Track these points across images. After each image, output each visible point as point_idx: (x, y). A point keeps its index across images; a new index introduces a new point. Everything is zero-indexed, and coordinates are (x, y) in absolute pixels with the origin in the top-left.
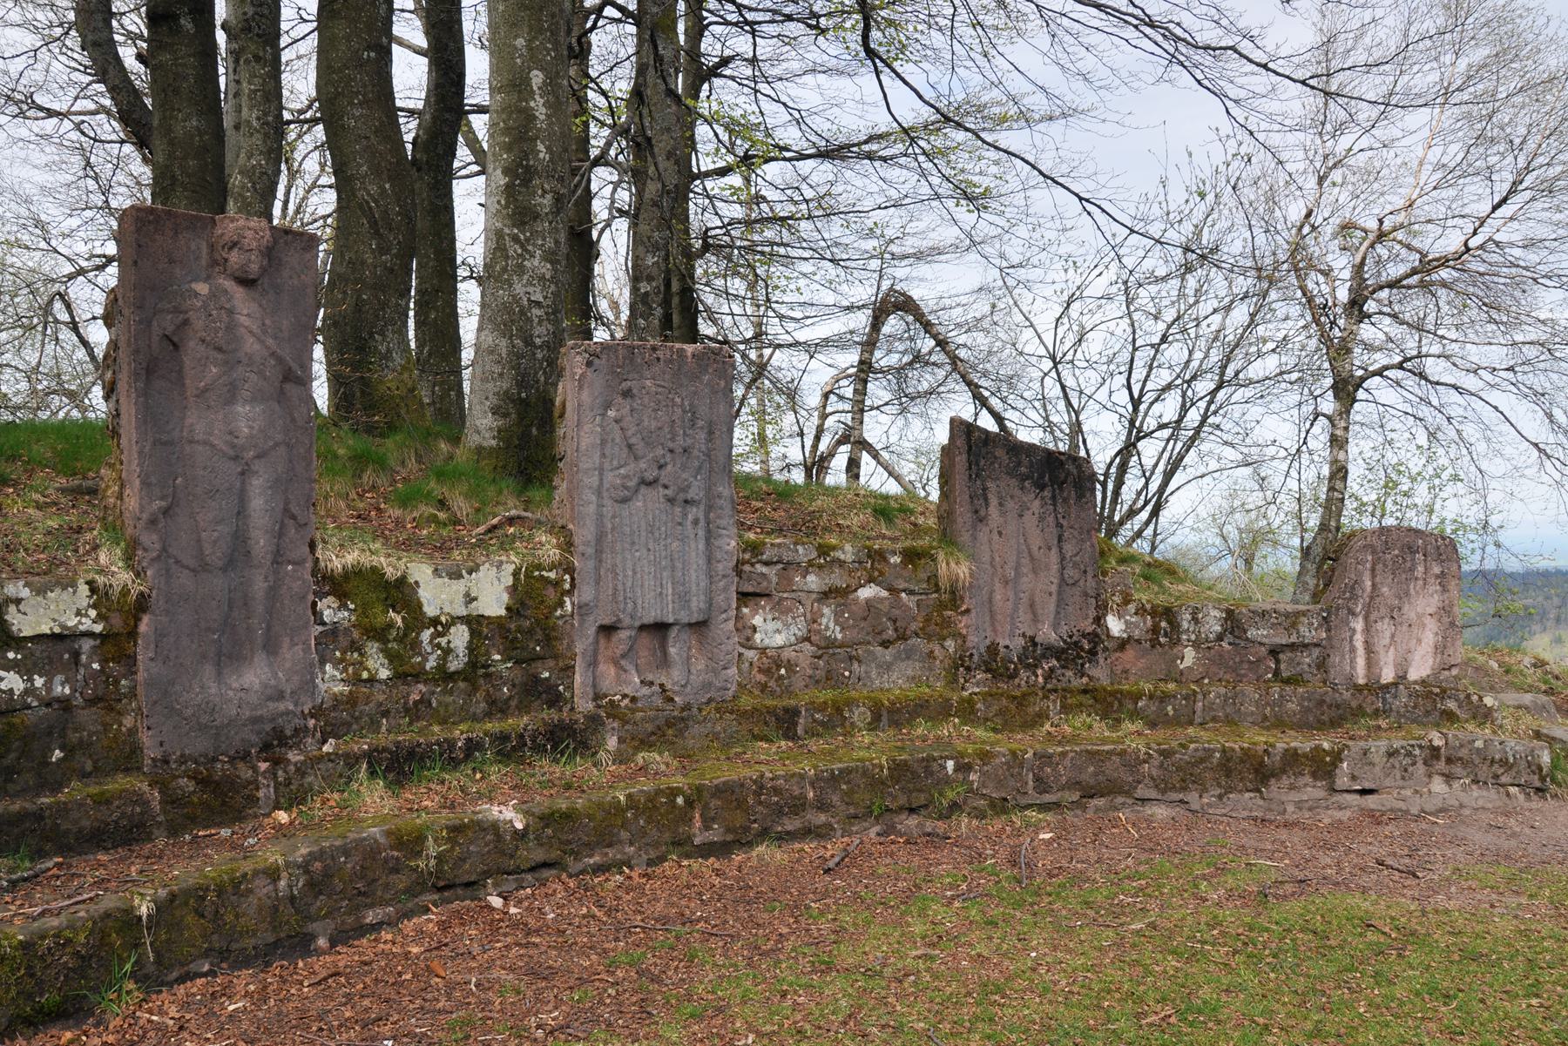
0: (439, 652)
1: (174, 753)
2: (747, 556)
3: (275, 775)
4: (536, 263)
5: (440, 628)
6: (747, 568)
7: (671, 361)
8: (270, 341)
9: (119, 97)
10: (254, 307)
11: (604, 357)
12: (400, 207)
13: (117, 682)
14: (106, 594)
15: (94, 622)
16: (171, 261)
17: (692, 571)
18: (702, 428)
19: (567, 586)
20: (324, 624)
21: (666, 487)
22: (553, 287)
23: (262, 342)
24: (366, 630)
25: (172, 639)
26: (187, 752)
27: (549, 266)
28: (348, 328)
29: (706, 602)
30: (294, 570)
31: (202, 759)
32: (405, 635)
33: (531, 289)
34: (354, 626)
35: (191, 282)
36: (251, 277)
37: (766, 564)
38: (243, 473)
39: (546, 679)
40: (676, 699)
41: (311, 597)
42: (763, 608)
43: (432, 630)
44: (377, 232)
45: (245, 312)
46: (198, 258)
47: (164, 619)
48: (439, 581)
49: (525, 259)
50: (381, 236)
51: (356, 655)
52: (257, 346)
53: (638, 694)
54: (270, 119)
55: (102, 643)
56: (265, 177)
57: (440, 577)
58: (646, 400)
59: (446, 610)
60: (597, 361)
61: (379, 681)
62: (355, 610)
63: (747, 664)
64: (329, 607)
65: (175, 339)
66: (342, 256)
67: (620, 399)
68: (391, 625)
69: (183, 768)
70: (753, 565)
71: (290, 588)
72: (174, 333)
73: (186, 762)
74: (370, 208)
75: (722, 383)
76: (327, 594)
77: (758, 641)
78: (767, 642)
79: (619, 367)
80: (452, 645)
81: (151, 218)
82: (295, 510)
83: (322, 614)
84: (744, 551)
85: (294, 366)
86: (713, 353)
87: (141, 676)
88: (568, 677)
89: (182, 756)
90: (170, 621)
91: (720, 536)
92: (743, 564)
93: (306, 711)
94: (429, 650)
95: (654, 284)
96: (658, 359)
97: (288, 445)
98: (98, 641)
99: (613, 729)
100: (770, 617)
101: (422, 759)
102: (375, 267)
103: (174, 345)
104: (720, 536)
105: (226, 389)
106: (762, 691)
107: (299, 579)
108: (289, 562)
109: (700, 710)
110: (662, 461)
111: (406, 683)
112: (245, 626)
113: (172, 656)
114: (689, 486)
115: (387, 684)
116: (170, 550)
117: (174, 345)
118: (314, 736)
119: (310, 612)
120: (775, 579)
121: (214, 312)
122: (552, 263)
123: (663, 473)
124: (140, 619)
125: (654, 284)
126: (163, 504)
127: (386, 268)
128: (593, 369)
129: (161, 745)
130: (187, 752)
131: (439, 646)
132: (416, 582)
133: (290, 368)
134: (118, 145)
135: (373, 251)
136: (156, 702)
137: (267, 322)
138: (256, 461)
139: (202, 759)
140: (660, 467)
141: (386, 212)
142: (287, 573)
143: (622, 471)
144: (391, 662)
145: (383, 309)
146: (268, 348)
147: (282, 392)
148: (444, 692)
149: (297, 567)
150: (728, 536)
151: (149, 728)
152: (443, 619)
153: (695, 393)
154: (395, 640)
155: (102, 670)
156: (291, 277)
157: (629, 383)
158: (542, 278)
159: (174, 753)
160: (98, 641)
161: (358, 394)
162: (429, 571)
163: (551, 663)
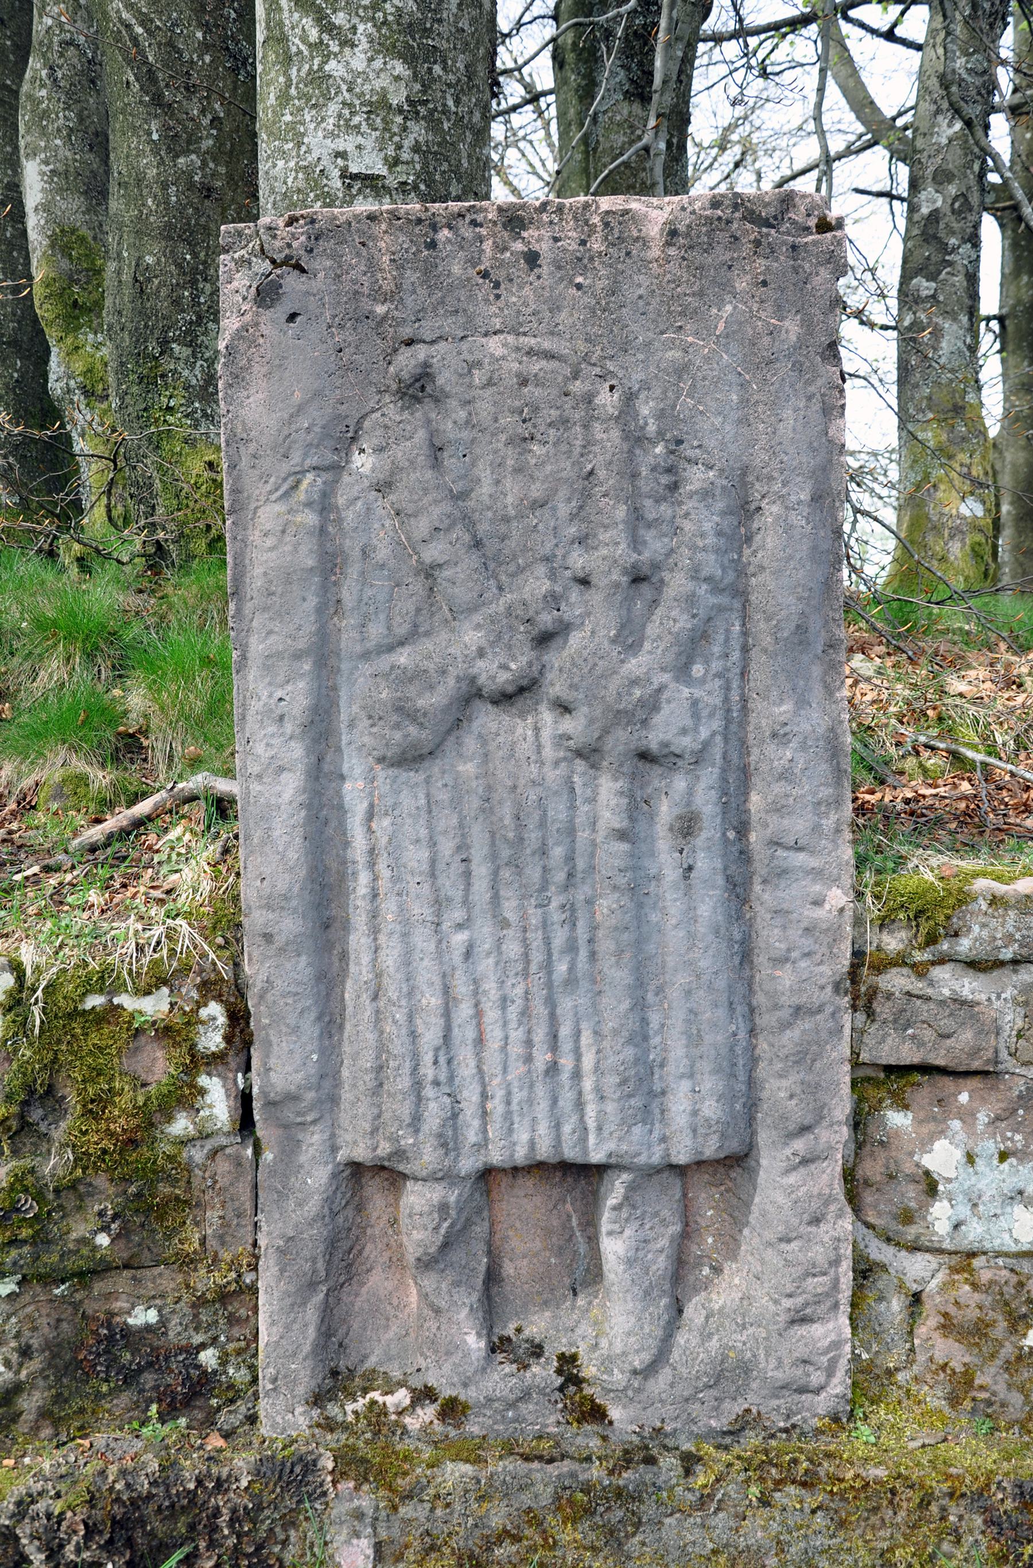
2: (893, 942)
4: (358, 61)
6: (897, 981)
7: (581, 262)
11: (320, 265)
12: (206, 28)
17: (674, 993)
18: (706, 494)
19: (212, 1040)
21: (564, 708)
22: (418, 132)
27: (399, 68)
29: (727, 1098)
33: (347, 143)
37: (974, 965)
39: (148, 1328)
40: (615, 1413)
42: (967, 1116)
49: (326, 59)
50: (168, 108)
53: (470, 1395)
56: (71, 51)
58: (484, 409)
60: (292, 281)
63: (896, 1304)
67: (392, 411)
70: (920, 971)
74: (135, 39)
75: (792, 328)
77: (942, 1228)
78: (974, 1232)
79: (379, 295)
84: (884, 923)
86: (752, 217)
88: (233, 1320)
91: (783, 872)
92: (881, 966)
95: (952, 190)
96: (532, 259)
99: (358, 1515)
100: (989, 1147)
102: (165, 186)
104: (783, 872)
106: (954, 1401)
109: (690, 1462)
110: (546, 619)
114: (652, 704)
120: (1012, 1019)
122: (409, 58)
123: (556, 658)
125: (952, 190)
127: (191, 185)
128: (281, 312)
140: (544, 639)
141: (171, 44)
143: (403, 658)
145: (194, 283)
150: (817, 874)
153: (681, 370)
157: (421, 352)
158: (379, 106)
163: (167, 1280)
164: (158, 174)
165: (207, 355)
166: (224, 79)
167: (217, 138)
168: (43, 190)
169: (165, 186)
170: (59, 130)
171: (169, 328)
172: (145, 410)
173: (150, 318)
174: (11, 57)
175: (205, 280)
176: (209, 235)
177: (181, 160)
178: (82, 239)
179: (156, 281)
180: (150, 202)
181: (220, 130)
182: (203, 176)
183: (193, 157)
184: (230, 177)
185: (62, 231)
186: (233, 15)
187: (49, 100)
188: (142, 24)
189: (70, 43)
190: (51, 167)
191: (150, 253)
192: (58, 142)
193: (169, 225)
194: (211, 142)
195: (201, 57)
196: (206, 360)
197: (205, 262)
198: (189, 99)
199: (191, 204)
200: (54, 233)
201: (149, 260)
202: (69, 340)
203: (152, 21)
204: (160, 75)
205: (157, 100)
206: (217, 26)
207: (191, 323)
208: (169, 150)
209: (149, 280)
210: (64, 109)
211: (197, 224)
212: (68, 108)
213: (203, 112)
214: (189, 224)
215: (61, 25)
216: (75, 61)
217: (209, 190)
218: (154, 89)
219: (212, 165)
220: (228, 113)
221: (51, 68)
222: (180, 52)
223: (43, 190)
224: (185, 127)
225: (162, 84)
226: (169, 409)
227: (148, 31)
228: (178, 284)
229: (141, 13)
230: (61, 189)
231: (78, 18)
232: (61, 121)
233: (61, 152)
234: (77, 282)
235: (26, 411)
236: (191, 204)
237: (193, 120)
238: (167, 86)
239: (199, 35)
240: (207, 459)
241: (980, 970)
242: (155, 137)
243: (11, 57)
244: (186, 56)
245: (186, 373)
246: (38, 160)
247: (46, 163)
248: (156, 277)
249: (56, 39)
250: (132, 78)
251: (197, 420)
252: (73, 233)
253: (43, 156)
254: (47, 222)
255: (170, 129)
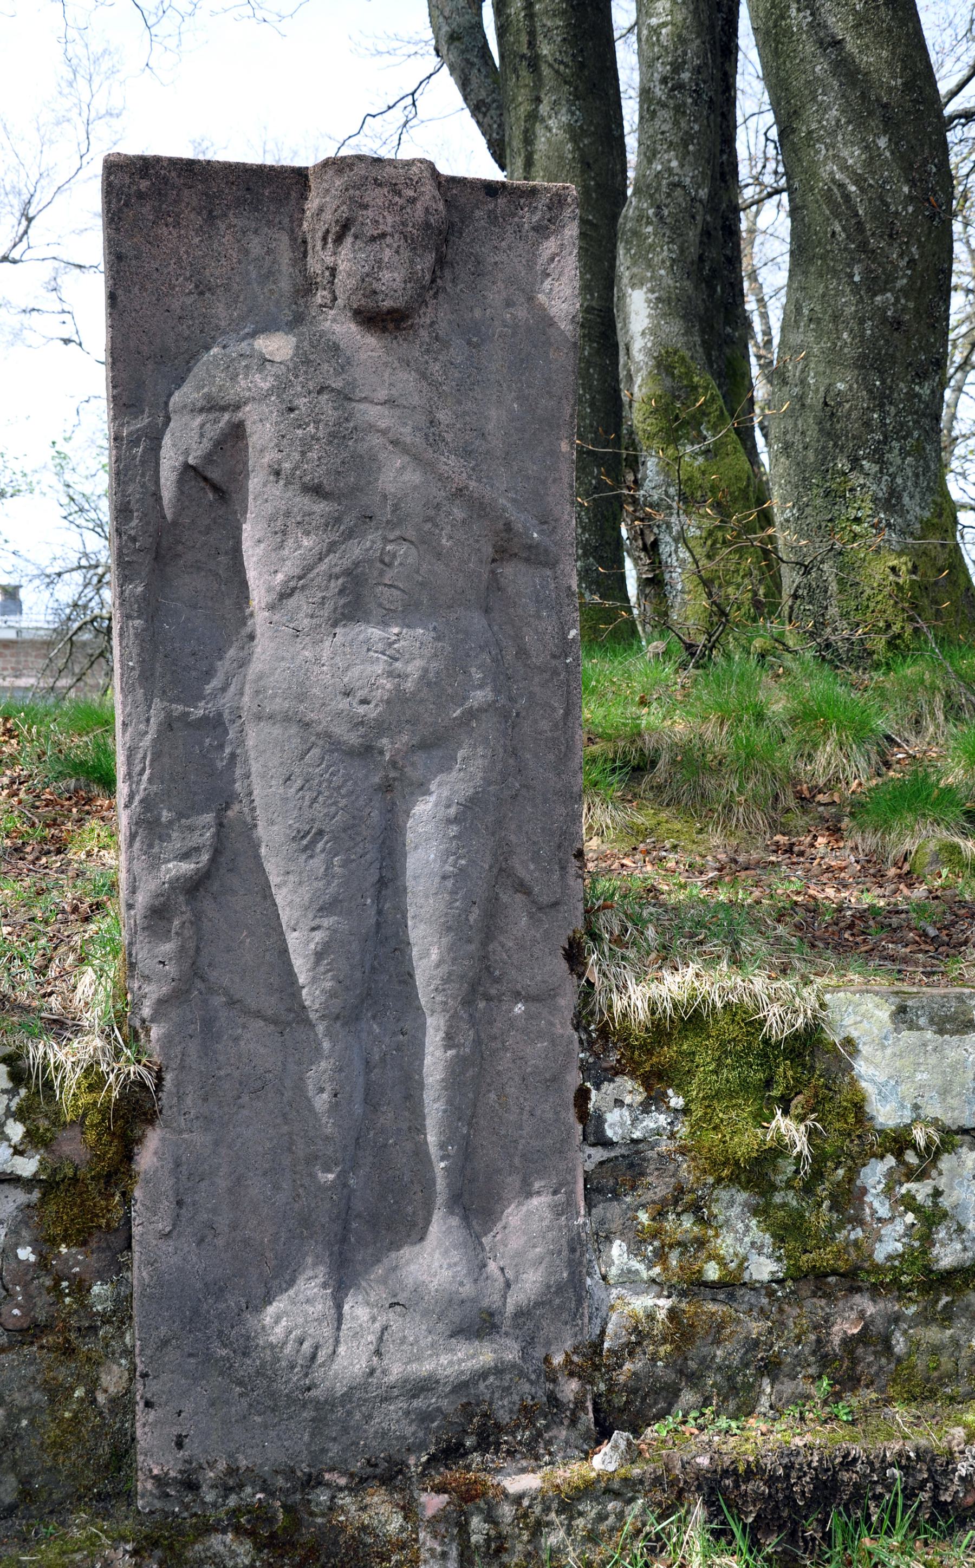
0: (910, 1218)
1: (212, 1465)
3: (464, 1528)
5: (911, 1157)
8: (450, 464)
9: (487, 120)
10: (407, 380)
12: (912, 183)
13: (81, 1288)
14: (48, 1085)
15: (18, 1152)
16: (203, 289)
20: (607, 1144)
23: (427, 466)
24: (714, 1163)
25: (223, 1184)
26: (243, 1463)
28: (811, 455)
30: (528, 1015)
31: (280, 1482)
32: (818, 1175)
34: (683, 1150)
35: (253, 335)
36: (387, 304)
38: (387, 787)
41: (574, 1079)
43: (890, 1161)
44: (863, 247)
45: (382, 394)
46: (269, 275)
47: (199, 1138)
48: (908, 1036)
50: (872, 254)
51: (687, 1222)
52: (413, 477)
54: (686, 76)
55: (43, 1200)
56: (678, 192)
57: (913, 1026)
59: (933, 1110)
61: (752, 1286)
62: (686, 1111)
64: (619, 1103)
65: (215, 474)
66: (798, 310)
68: (779, 1150)
69: (232, 1501)
71: (519, 1059)
72: (208, 458)
73: (241, 1486)
74: (847, 197)
76: (614, 1073)
80: (945, 1202)
81: (144, 184)
82: (525, 869)
83: (600, 1120)
85: (520, 519)
87: (139, 1275)
89: (232, 1471)
90: (216, 1143)
93: (558, 1360)
94: (883, 1211)
97: (505, 715)
98: (36, 1195)
101: (857, 1497)
102: (862, 321)
103: (216, 488)
105: (336, 585)
107: (540, 1035)
108: (517, 996)
111: (823, 1292)
112: (409, 1146)
113: (222, 1223)
115: (771, 1294)
116: (213, 975)
117: (216, 488)
118: (574, 1422)
119: (571, 1115)
121: (301, 402)
124: (139, 1141)
126: (187, 867)
127: (884, 320)
129: (180, 1445)
130: (243, 1463)
131: (909, 1203)
132: (848, 1041)
133: (508, 527)
134: (962, 395)
135: (856, 288)
136: (165, 1343)
137: (443, 416)
138: (420, 758)
139: (280, 1482)
141: (881, 198)
142: (512, 1022)
144: (779, 1239)
145: (882, 405)
146: (443, 479)
147: (495, 585)
148: (925, 1318)
149: (535, 1007)
151: (148, 1404)
152: (919, 1135)
154: (789, 1186)
155: (43, 1263)
156: (509, 304)
159: (212, 1465)
160: (36, 1195)
161: (834, 587)
162: (883, 1013)
164: (856, 311)
165: (891, 470)
166: (922, 225)
167: (910, 277)
168: (649, 316)
169: (862, 321)
170: (663, 262)
171: (859, 447)
172: (830, 520)
173: (840, 438)
174: (594, 195)
175: (891, 403)
176: (895, 363)
177: (878, 298)
178: (683, 359)
179: (847, 406)
180: (845, 335)
181: (914, 270)
182: (895, 311)
183: (889, 295)
184: (917, 310)
185: (667, 352)
186: (934, 170)
187: (655, 235)
188: (856, 183)
189: (678, 185)
190: (656, 295)
191: (842, 380)
192: (662, 272)
193: (862, 356)
194: (905, 281)
195: (905, 208)
196: (890, 476)
197: (891, 388)
198: (890, 245)
199: (883, 336)
200: (660, 355)
201: (841, 386)
202: (670, 451)
203: (865, 180)
204: (868, 226)
205: (863, 247)
206: (921, 180)
207: (879, 442)
208: (869, 289)
209: (840, 404)
210: (668, 243)
211: (886, 354)
212: (672, 241)
213: (901, 256)
214: (879, 354)
215: (670, 170)
216: (681, 200)
217: (899, 323)
218: (860, 238)
219: (903, 301)
220: (921, 256)
221: (659, 207)
222: (887, 205)
223: (649, 316)
224: (884, 269)
225: (869, 233)
226: (857, 520)
227: (862, 190)
228: (868, 408)
229: (856, 174)
230: (665, 314)
231: (686, 162)
232: (665, 253)
233: (664, 281)
234: (678, 398)
235: (602, 514)
236: (883, 336)
237: (892, 262)
238: (873, 234)
239: (906, 189)
240: (890, 564)
241: (468, 1002)
242: (857, 278)
243: (594, 195)
244: (892, 208)
245: (874, 487)
246: (645, 289)
247: (652, 291)
248: (847, 401)
249: (664, 182)
250: (838, 229)
251: (881, 529)
252: (675, 354)
253: (649, 285)
254: (654, 345)
255: (871, 272)
